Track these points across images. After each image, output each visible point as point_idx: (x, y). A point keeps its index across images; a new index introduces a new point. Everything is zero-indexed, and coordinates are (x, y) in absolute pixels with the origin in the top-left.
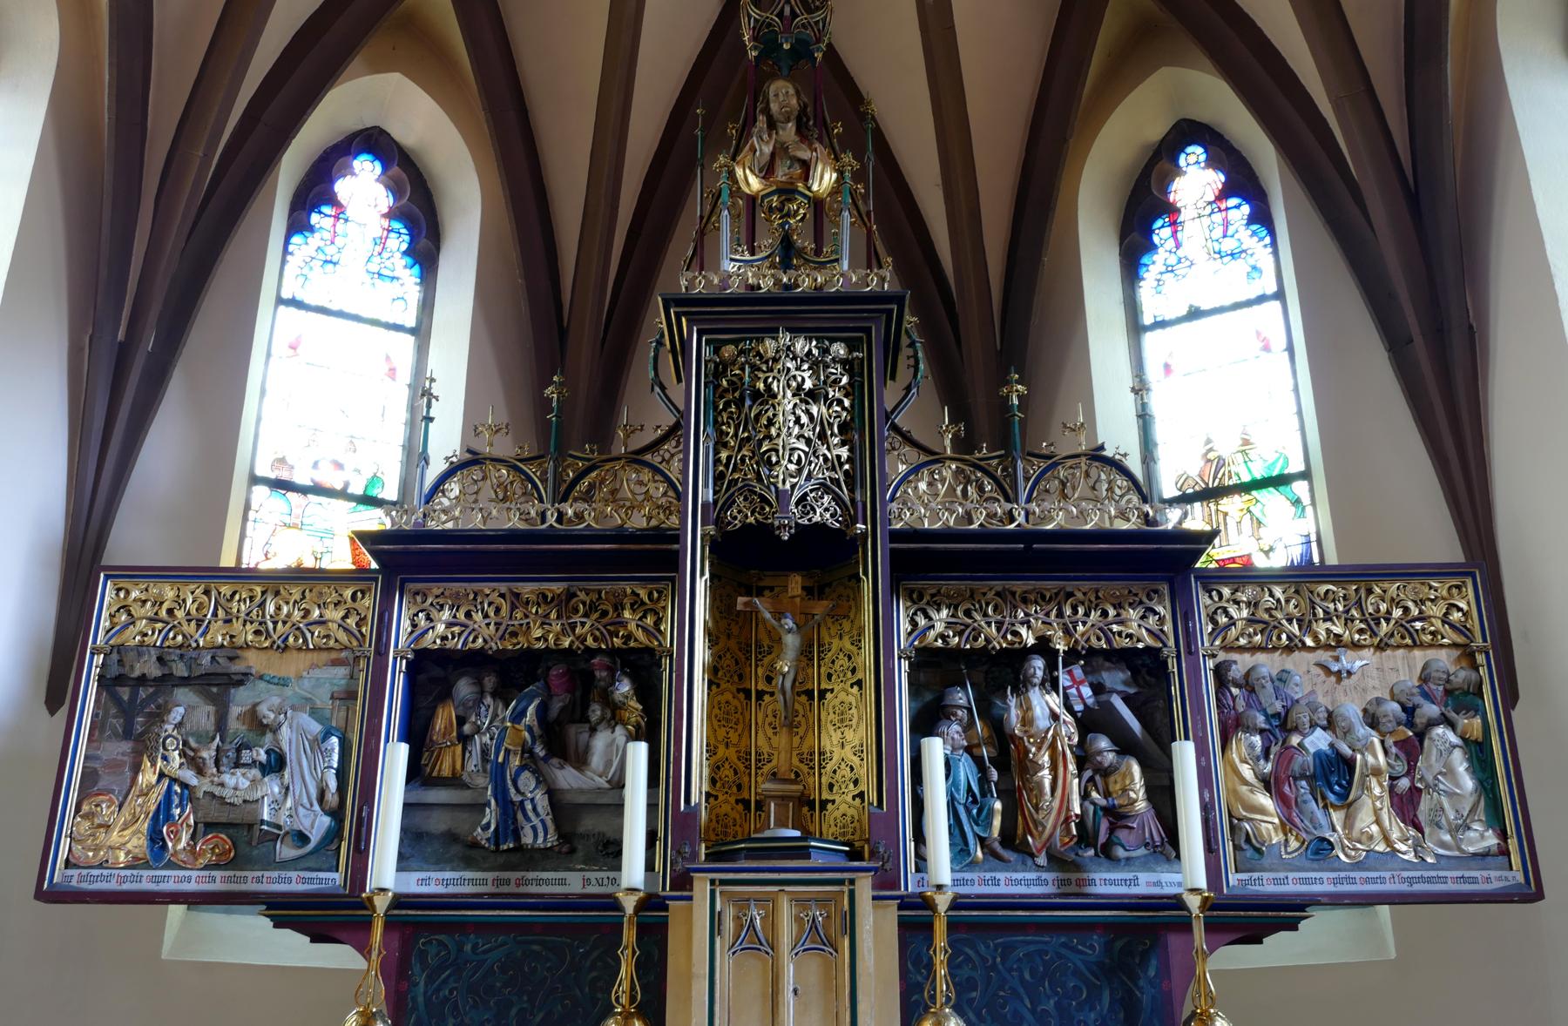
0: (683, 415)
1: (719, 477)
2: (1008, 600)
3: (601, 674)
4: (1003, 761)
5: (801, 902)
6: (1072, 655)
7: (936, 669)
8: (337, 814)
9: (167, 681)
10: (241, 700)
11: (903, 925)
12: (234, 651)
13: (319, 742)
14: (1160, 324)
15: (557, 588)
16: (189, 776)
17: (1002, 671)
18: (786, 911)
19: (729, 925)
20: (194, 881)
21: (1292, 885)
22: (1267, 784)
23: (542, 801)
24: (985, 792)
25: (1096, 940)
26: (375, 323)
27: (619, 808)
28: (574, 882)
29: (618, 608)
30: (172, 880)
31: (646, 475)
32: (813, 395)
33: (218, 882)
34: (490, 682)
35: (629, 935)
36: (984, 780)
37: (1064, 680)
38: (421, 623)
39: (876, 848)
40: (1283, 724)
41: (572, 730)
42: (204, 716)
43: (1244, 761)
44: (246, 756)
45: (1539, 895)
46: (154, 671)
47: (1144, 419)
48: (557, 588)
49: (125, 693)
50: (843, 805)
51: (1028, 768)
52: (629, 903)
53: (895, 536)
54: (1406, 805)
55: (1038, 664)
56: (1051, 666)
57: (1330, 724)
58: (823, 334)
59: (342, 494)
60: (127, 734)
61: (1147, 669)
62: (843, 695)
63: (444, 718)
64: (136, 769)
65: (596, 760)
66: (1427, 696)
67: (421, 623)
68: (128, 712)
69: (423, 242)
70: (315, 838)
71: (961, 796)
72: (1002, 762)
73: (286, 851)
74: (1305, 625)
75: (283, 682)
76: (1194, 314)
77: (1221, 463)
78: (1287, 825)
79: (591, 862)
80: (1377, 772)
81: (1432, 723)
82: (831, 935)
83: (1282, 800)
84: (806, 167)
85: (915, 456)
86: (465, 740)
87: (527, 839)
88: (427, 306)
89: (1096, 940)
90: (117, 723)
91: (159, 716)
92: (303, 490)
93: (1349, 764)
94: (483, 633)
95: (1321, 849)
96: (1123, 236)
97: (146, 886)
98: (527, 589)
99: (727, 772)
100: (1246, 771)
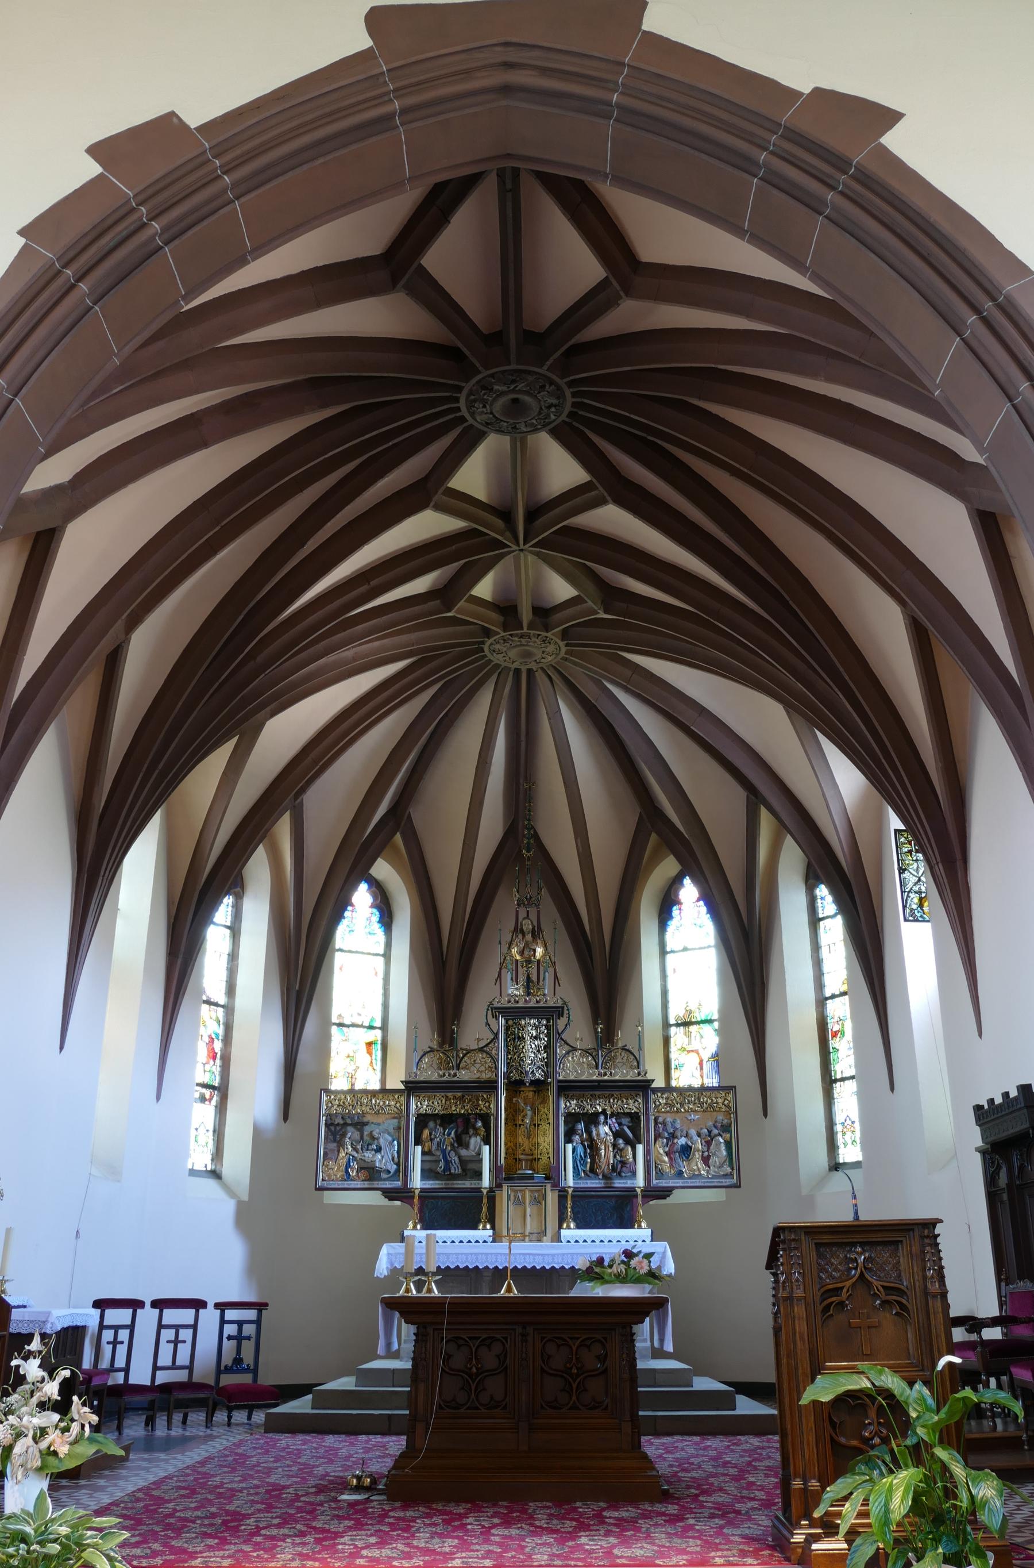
0: (496, 1035)
1: (508, 1063)
2: (593, 1097)
3: (473, 1120)
4: (592, 1147)
5: (531, 1191)
6: (612, 1115)
7: (572, 1119)
8: (398, 1164)
9: (346, 1124)
10: (367, 1130)
11: (559, 1196)
12: (364, 1114)
13: (391, 1143)
14: (672, 952)
15: (459, 1094)
16: (356, 1155)
17: (592, 1120)
18: (527, 1194)
19: (512, 1198)
20: (359, 1184)
21: (671, 1183)
22: (667, 1154)
23: (456, 1159)
24: (585, 1156)
25: (613, 1200)
26: (369, 954)
27: (481, 1161)
28: (467, 1184)
29: (478, 1100)
30: (353, 1184)
31: (485, 1055)
32: (536, 1038)
33: (366, 1185)
34: (438, 1122)
35: (485, 1200)
36: (585, 1153)
37: (609, 1121)
38: (417, 1106)
39: (553, 1176)
40: (673, 1136)
41: (464, 1136)
42: (357, 1135)
43: (659, 1149)
44: (370, 1147)
45: (739, 1186)
46: (342, 1122)
47: (664, 993)
48: (459, 1094)
49: (332, 1128)
50: (544, 1160)
51: (598, 1149)
52: (485, 1192)
53: (559, 1081)
54: (706, 1160)
55: (602, 1118)
56: (606, 1118)
57: (687, 1136)
58: (539, 1018)
59: (362, 1026)
60: (335, 1141)
61: (634, 1117)
62: (544, 1126)
63: (426, 1132)
64: (339, 1151)
65: (472, 1146)
66: (715, 1127)
67: (417, 1106)
68: (334, 1134)
69: (386, 919)
70: (392, 1171)
71: (578, 1158)
72: (591, 1147)
73: (384, 1176)
74: (682, 1105)
75: (379, 1124)
76: (685, 949)
77: (691, 1012)
78: (671, 1166)
79: (472, 1178)
80: (698, 1150)
81: (716, 1136)
82: (540, 1200)
83: (670, 1158)
84: (535, 951)
85: (567, 1048)
86: (431, 1140)
87: (453, 1171)
88: (388, 945)
89: (613, 1200)
90: (331, 1137)
91: (344, 1135)
92: (348, 1026)
93: (691, 1148)
94: (438, 1110)
95: (680, 1174)
96: (660, 916)
97: (346, 1186)
98: (449, 1094)
99: (510, 1150)
100: (661, 1151)
